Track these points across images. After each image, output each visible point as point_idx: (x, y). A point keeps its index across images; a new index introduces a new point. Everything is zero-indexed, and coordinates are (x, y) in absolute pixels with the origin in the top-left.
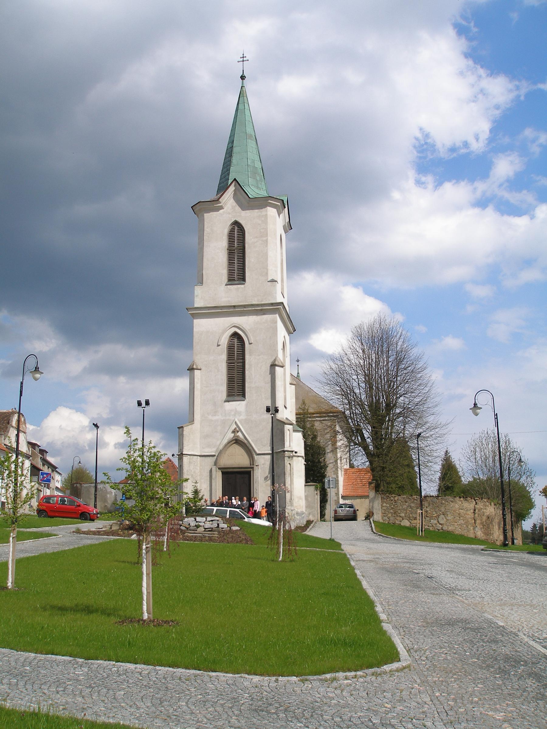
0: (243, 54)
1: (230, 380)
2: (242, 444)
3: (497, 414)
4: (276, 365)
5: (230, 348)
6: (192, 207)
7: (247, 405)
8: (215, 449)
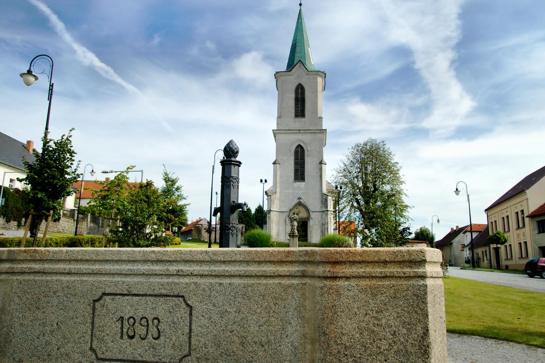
1: (296, 171)
3: (53, 84)
4: (322, 163)
5: (296, 152)
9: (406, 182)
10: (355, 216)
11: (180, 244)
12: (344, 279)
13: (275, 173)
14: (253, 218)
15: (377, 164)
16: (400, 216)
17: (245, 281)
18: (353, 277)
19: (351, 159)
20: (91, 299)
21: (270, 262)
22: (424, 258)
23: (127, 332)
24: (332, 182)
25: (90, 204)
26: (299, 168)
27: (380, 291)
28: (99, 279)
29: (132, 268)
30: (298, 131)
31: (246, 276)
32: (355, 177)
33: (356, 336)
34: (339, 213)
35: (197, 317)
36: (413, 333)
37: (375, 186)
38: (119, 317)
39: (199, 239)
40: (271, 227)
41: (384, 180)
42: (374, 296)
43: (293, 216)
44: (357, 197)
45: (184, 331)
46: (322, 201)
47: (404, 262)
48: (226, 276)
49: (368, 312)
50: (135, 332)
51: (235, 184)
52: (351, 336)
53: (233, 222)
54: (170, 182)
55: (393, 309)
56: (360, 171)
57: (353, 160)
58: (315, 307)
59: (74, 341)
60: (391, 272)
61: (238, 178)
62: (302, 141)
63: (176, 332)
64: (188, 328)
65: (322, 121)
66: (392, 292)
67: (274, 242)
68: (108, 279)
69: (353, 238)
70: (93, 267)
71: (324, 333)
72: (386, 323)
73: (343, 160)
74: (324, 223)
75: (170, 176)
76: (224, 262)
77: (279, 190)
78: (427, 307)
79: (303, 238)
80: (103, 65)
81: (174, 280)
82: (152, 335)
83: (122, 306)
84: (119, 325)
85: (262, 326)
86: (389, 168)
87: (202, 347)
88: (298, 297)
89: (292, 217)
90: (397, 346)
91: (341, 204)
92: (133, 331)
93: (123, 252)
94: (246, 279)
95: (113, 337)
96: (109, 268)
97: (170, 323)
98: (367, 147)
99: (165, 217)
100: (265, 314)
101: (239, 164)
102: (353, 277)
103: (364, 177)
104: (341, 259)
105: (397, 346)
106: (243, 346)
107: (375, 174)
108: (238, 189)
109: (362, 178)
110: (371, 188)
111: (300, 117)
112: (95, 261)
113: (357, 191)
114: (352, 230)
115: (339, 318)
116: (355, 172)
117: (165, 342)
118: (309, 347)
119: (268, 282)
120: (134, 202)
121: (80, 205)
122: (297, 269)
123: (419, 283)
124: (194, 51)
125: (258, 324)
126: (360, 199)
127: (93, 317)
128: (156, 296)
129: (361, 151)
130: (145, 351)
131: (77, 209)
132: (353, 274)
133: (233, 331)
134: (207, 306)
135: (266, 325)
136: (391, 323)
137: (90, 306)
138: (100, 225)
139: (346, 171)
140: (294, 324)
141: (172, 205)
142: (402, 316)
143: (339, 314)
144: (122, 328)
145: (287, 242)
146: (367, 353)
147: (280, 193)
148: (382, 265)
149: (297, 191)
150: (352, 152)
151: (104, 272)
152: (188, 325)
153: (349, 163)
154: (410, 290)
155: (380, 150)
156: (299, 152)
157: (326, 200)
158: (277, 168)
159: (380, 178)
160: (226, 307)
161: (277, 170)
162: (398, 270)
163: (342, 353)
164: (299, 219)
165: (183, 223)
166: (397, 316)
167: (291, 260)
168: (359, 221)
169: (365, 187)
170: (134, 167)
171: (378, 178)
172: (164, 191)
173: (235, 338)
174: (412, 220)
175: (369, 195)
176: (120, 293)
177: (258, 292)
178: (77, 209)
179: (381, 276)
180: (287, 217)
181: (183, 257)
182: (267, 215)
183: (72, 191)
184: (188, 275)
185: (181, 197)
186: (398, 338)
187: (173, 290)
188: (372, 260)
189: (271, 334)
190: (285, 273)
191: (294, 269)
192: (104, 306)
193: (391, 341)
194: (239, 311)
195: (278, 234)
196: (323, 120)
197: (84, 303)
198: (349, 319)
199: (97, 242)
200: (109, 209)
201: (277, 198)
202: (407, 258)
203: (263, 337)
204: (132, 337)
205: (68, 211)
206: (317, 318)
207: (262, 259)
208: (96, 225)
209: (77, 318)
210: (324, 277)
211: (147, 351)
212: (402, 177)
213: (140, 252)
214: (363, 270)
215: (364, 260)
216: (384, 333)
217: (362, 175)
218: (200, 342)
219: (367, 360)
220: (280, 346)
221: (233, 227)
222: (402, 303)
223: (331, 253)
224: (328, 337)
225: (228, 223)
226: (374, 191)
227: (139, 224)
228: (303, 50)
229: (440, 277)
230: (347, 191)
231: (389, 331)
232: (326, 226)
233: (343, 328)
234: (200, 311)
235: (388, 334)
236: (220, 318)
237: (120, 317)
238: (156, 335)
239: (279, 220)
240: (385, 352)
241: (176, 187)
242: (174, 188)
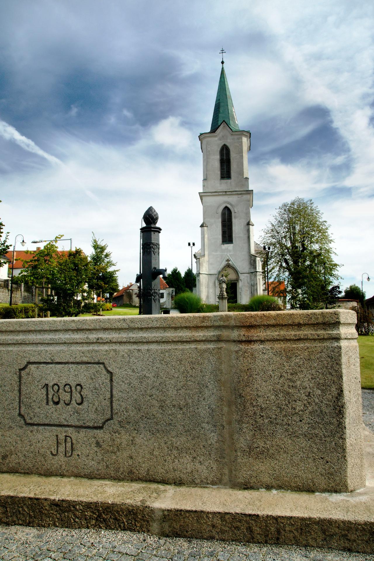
4: (250, 225)
5: (223, 214)
7: (233, 246)
8: (216, 271)
9: (335, 241)
10: (284, 276)
11: (111, 309)
12: (259, 343)
13: (203, 236)
14: (183, 282)
15: (305, 223)
16: (329, 275)
17: (162, 347)
18: (268, 340)
19: (279, 219)
20: (17, 368)
21: (186, 327)
22: (338, 320)
23: (52, 398)
24: (260, 242)
25: (21, 275)
26: (227, 230)
27: (294, 353)
28: (23, 348)
29: (53, 337)
30: (224, 193)
31: (163, 342)
32: (283, 237)
33: (272, 398)
34: (268, 273)
35: (117, 383)
36: (327, 394)
37: (303, 245)
38: (44, 384)
39: (130, 304)
40: (201, 290)
41: (312, 239)
42: (289, 358)
43: (221, 278)
44: (285, 257)
45: (105, 396)
46: (251, 262)
47: (318, 324)
48: (144, 343)
49: (282, 374)
50: (59, 398)
51: (155, 251)
52: (266, 398)
53: (155, 289)
54: (99, 249)
55: (308, 371)
56: (288, 230)
57: (281, 220)
58: (231, 371)
59: (4, 408)
60: (305, 335)
61: (159, 245)
62: (228, 203)
63: (98, 397)
64: (109, 393)
65: (248, 181)
66: (306, 354)
67: (203, 305)
68: (31, 348)
69: (282, 298)
70: (17, 338)
71: (240, 395)
72: (301, 385)
73: (270, 221)
74: (253, 284)
75: (98, 243)
76: (141, 329)
77: (207, 252)
78: (341, 368)
79: (232, 299)
80: (23, 138)
81: (94, 348)
82: (76, 401)
83: (46, 374)
84: (44, 391)
85: (180, 389)
86: (317, 227)
87: (123, 411)
88: (214, 361)
89: (221, 279)
90: (312, 407)
91: (269, 265)
92: (58, 397)
93: (45, 322)
94: (163, 345)
95: (39, 403)
96: (32, 338)
97: (92, 389)
98: (294, 206)
99: (95, 284)
100: (182, 378)
101: (159, 230)
102: (268, 340)
103: (292, 236)
104: (255, 323)
105: (312, 407)
106: (162, 409)
107: (303, 234)
108: (159, 255)
109: (290, 238)
110: (300, 247)
111: (225, 179)
112: (19, 332)
113: (285, 251)
114: (281, 291)
115: (254, 381)
116: (284, 232)
117: (89, 407)
118: (226, 409)
119: (185, 347)
120: (62, 271)
121: (13, 275)
122: (212, 334)
123: (333, 345)
124: (112, 120)
125: (176, 388)
126: (288, 259)
127: (20, 385)
128: (78, 363)
129: (289, 211)
130: (70, 416)
131: (10, 279)
132: (267, 338)
133: (152, 395)
134: (126, 372)
135: (184, 389)
136: (306, 384)
137: (17, 374)
138: (34, 293)
139: (274, 230)
140: (210, 387)
141: (102, 272)
142: (316, 378)
143: (255, 376)
144: (47, 394)
145: (217, 304)
146: (282, 414)
147: (209, 255)
148: (296, 327)
149: (226, 253)
150: (279, 212)
151: (28, 342)
152: (109, 390)
153: (276, 223)
154: (324, 352)
155: (308, 209)
156: (227, 214)
157: (255, 261)
158: (205, 231)
159: (308, 237)
160: (144, 373)
161: (205, 233)
162: (312, 333)
163: (258, 414)
164: (228, 281)
165: (115, 289)
166: (311, 378)
167: (206, 325)
168: (288, 281)
169: (294, 246)
170: (62, 236)
171: (307, 237)
172: (94, 259)
173: (154, 401)
174: (341, 278)
175: (297, 255)
176: (43, 361)
177: (175, 358)
178: (10, 279)
179: (295, 338)
180: (217, 279)
181: (102, 325)
182: (197, 278)
183: (2, 263)
184: (107, 342)
185: (110, 264)
186: (312, 399)
187: (94, 357)
188: (286, 323)
189: (189, 397)
190: (201, 338)
191: (210, 334)
192: (29, 374)
193: (306, 402)
194: (157, 376)
195: (208, 297)
196: (249, 180)
197: (10, 372)
198: (264, 382)
199: (31, 311)
200: (41, 278)
201: (205, 261)
202: (320, 320)
203: (181, 400)
204: (57, 403)
205: (2, 281)
206: (233, 381)
207: (178, 325)
208: (30, 294)
209: (5, 386)
210: (239, 341)
211: (72, 416)
212: (331, 235)
213: (60, 321)
214: (277, 333)
215: (278, 323)
216: (299, 395)
217: (291, 234)
218: (121, 407)
219: (283, 420)
220: (198, 408)
221: (155, 293)
222: (316, 364)
223: (246, 317)
224: (244, 400)
225: (150, 289)
226: (303, 251)
227: (69, 292)
228: (227, 110)
229: (355, 339)
230: (276, 252)
231: (304, 393)
232: (256, 287)
233: (258, 390)
234: (120, 377)
235: (303, 395)
236: (139, 383)
237: (45, 384)
238: (79, 401)
239: (208, 283)
240: (300, 413)
241: (105, 253)
242: (103, 255)
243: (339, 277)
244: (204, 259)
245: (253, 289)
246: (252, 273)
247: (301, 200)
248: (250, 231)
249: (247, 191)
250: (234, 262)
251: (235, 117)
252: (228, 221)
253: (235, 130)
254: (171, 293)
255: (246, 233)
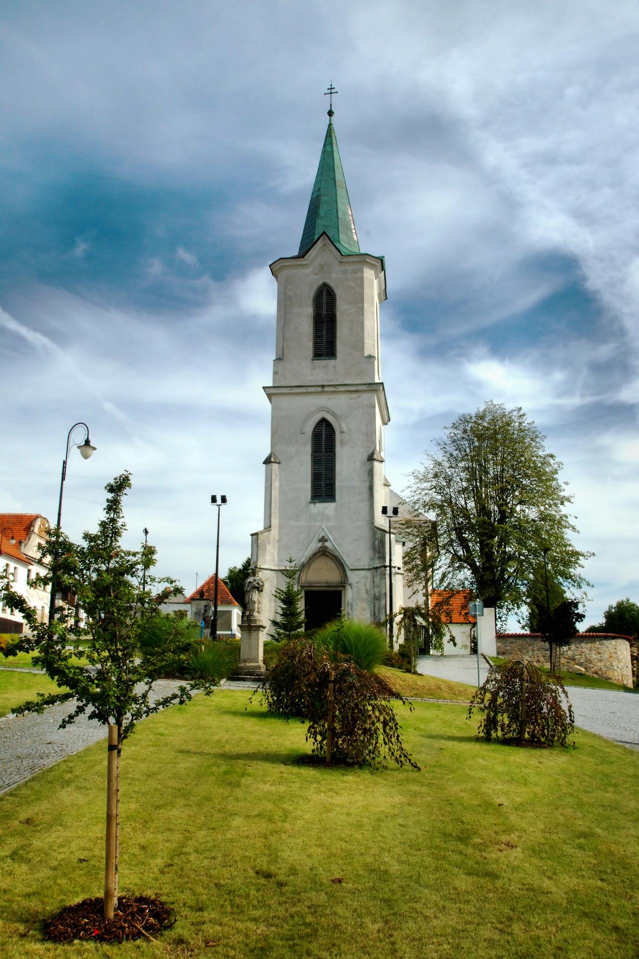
0: (331, 85)
1: (316, 477)
2: (330, 556)
4: (374, 459)
6: (270, 266)
9: (572, 500)
26: (323, 472)
30: (319, 389)
62: (329, 411)
74: (377, 594)
124: (156, 268)
147: (281, 526)
149: (318, 524)
150: (453, 435)
156: (324, 435)
161: (274, 476)
169: (483, 510)
174: (588, 584)
212: (564, 486)
232: (383, 603)
243: (584, 582)
244: (268, 537)
245: (377, 607)
246: (376, 568)
247: (497, 407)
248: (375, 474)
249: (370, 384)
250: (337, 545)
251: (353, 227)
252: (326, 452)
253: (348, 253)
254: (203, 612)
255: (366, 478)
